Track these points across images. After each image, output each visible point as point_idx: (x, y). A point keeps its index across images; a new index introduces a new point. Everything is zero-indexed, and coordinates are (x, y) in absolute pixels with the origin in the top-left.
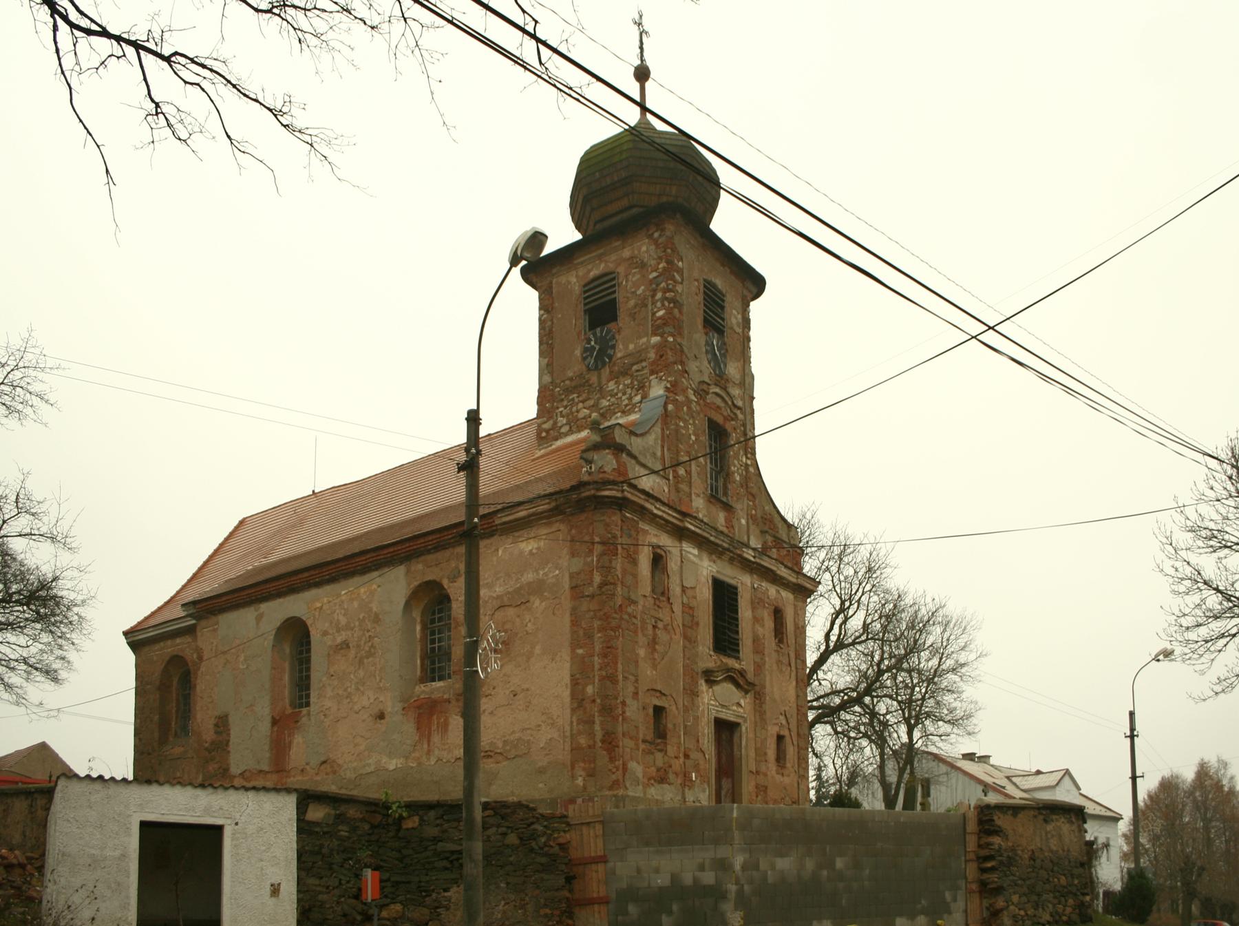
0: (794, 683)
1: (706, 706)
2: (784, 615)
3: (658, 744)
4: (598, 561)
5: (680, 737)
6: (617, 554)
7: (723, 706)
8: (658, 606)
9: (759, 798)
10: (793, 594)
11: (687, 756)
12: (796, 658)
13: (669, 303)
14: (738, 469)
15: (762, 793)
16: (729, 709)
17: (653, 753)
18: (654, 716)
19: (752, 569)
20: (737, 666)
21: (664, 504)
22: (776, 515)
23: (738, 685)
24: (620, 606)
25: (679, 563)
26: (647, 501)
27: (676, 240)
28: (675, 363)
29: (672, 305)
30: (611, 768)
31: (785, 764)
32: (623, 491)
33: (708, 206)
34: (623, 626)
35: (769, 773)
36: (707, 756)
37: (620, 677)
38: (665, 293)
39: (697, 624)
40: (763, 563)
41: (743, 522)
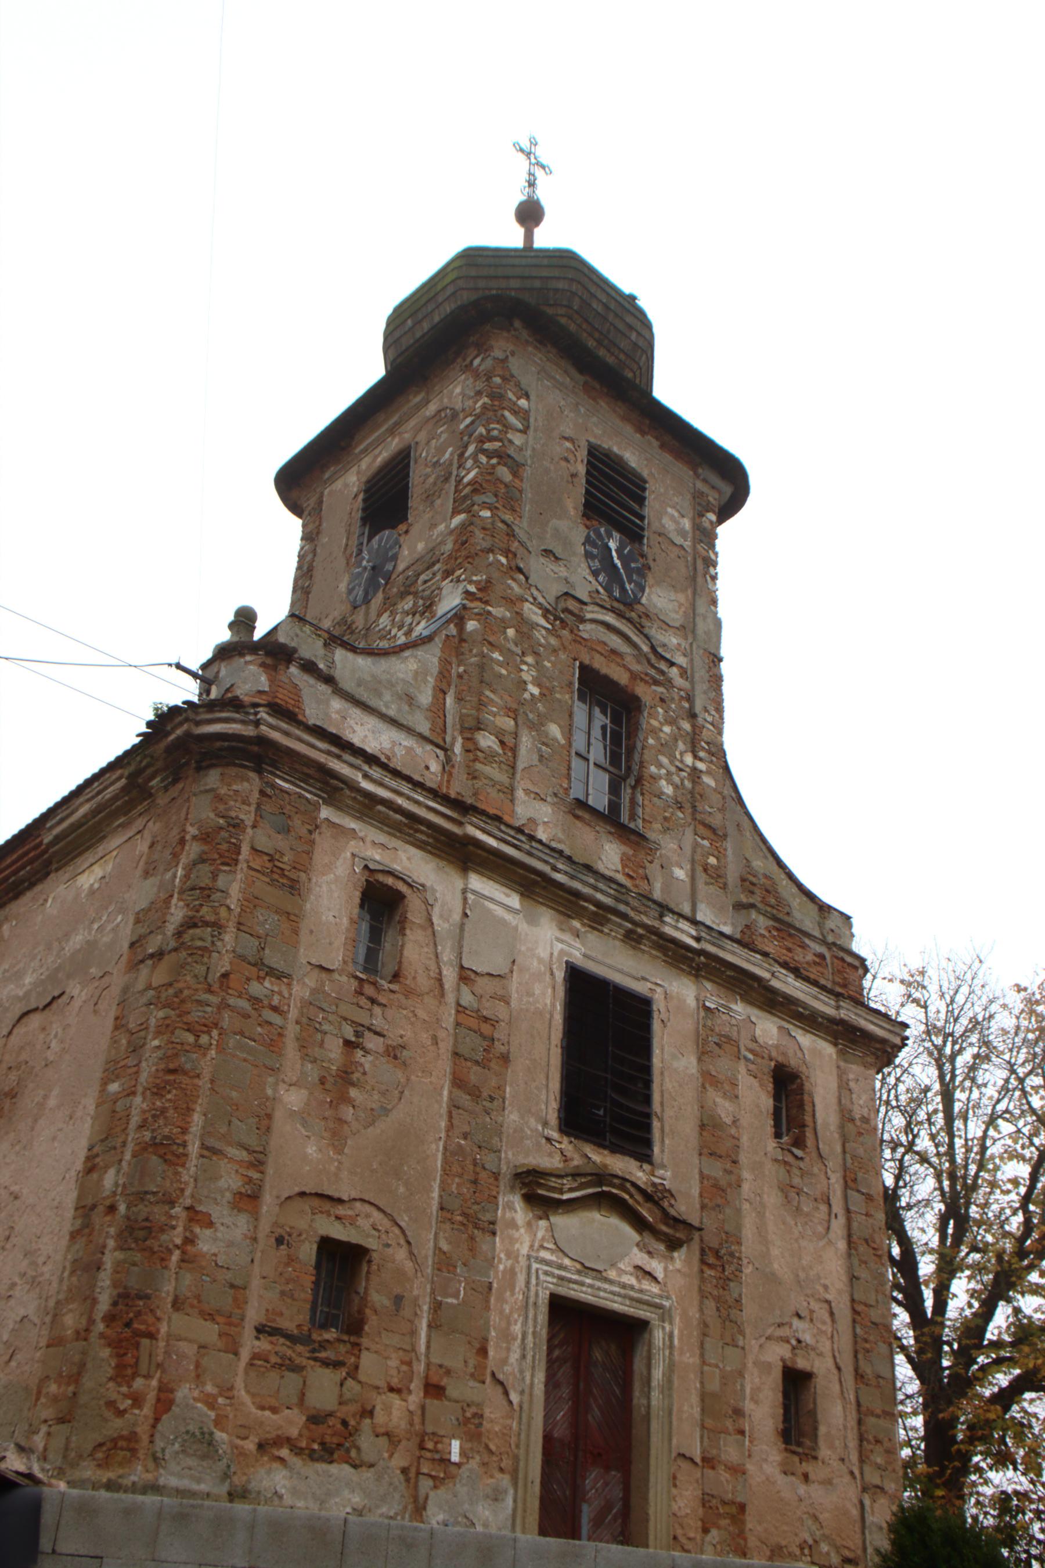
0: (842, 1245)
1: (523, 1261)
2: (807, 1086)
3: (323, 1345)
4: (187, 876)
5: (414, 1333)
6: (236, 862)
7: (586, 1269)
8: (373, 1001)
9: (714, 1534)
10: (835, 1045)
11: (434, 1390)
12: (846, 1186)
13: (490, 458)
14: (669, 773)
15: (724, 1522)
16: (606, 1280)
17: (297, 1369)
18: (318, 1266)
19: (698, 969)
20: (639, 1174)
21: (396, 773)
22: (785, 882)
23: (639, 1223)
24: (225, 976)
25: (457, 917)
26: (339, 757)
27: (515, 365)
28: (490, 550)
29: (494, 461)
30: (114, 1396)
31: (815, 1447)
32: (257, 723)
33: (622, 357)
34: (225, 1024)
35: (750, 1467)
36: (514, 1397)
37: (194, 1148)
38: (483, 442)
39: (505, 1059)
40: (722, 954)
41: (680, 874)
